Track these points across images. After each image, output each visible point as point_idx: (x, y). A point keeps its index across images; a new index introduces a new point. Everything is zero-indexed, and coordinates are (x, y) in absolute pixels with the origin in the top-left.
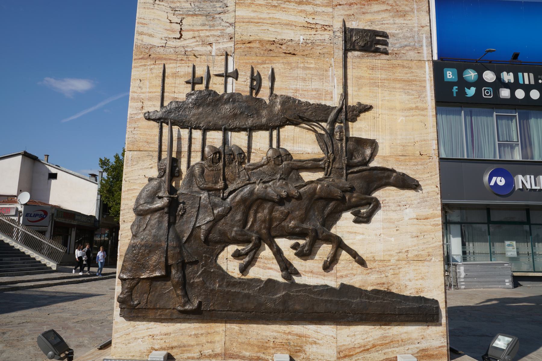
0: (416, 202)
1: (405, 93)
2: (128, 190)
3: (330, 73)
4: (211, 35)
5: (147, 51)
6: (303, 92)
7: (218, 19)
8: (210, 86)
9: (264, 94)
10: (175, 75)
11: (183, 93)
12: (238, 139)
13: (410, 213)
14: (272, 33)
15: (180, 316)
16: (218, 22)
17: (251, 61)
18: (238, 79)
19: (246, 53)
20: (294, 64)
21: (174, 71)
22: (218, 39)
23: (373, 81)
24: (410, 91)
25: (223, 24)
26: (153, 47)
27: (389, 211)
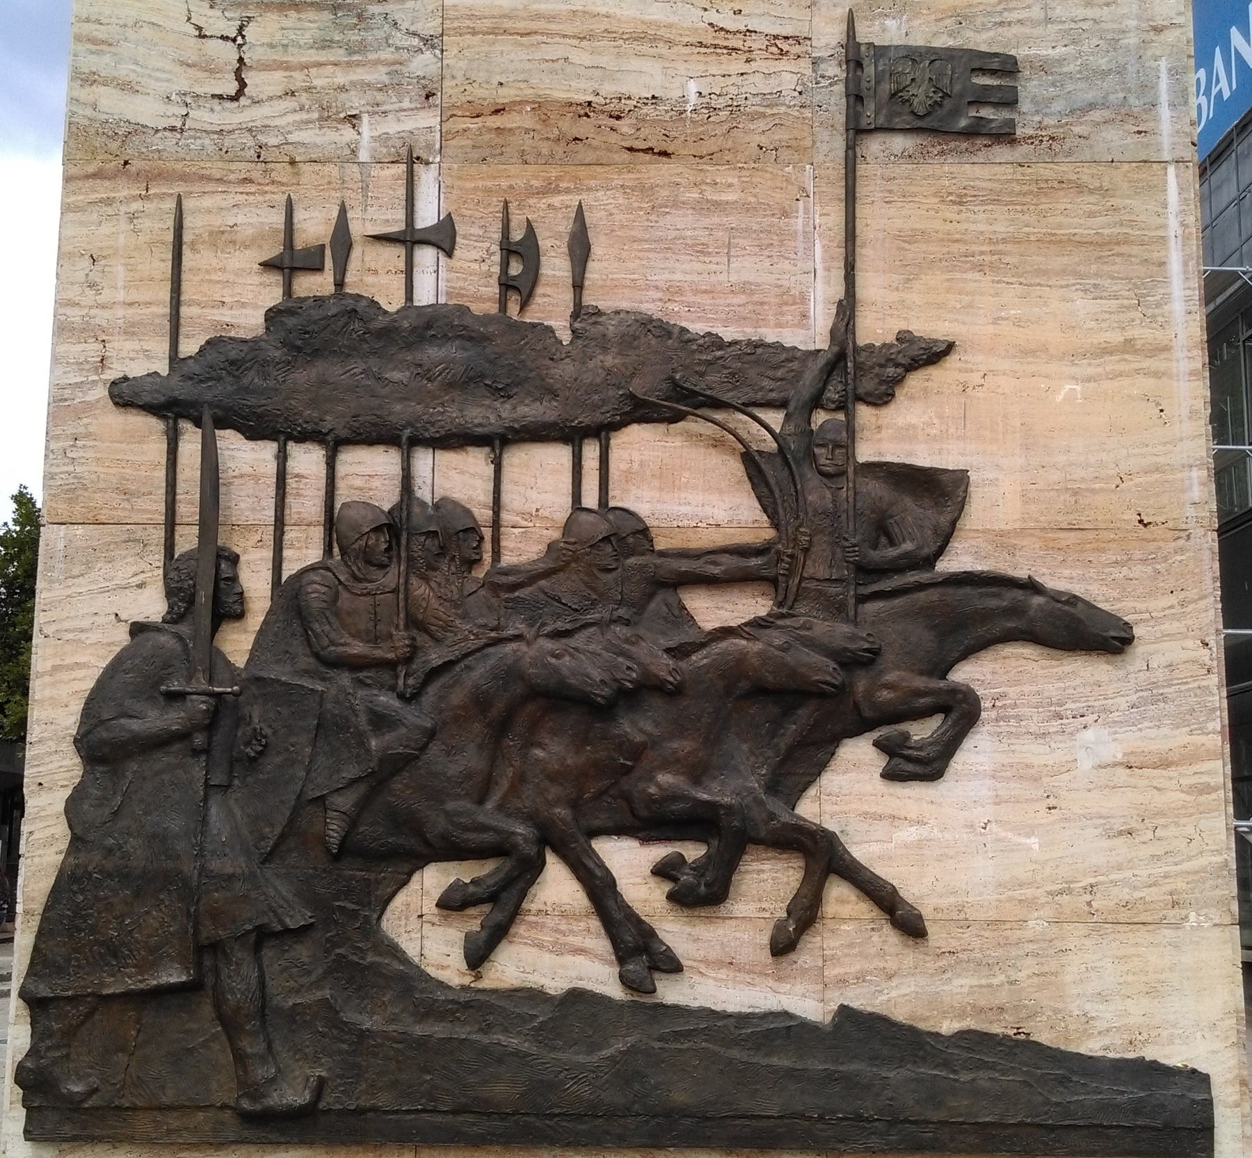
0: (1122, 702)
1: (1085, 291)
2: (56, 668)
3: (799, 223)
4: (353, 84)
5: (113, 146)
6: (698, 299)
7: (379, 20)
8: (349, 278)
9: (551, 308)
10: (223, 239)
11: (256, 307)
12: (454, 477)
13: (1099, 743)
14: (582, 71)
15: (246, 1133)
16: (380, 34)
17: (504, 184)
18: (457, 253)
19: (486, 152)
20: (665, 193)
21: (217, 222)
22: (380, 97)
23: (963, 248)
24: (1106, 283)
25: (399, 39)
26: (138, 129)
27: (1018, 736)
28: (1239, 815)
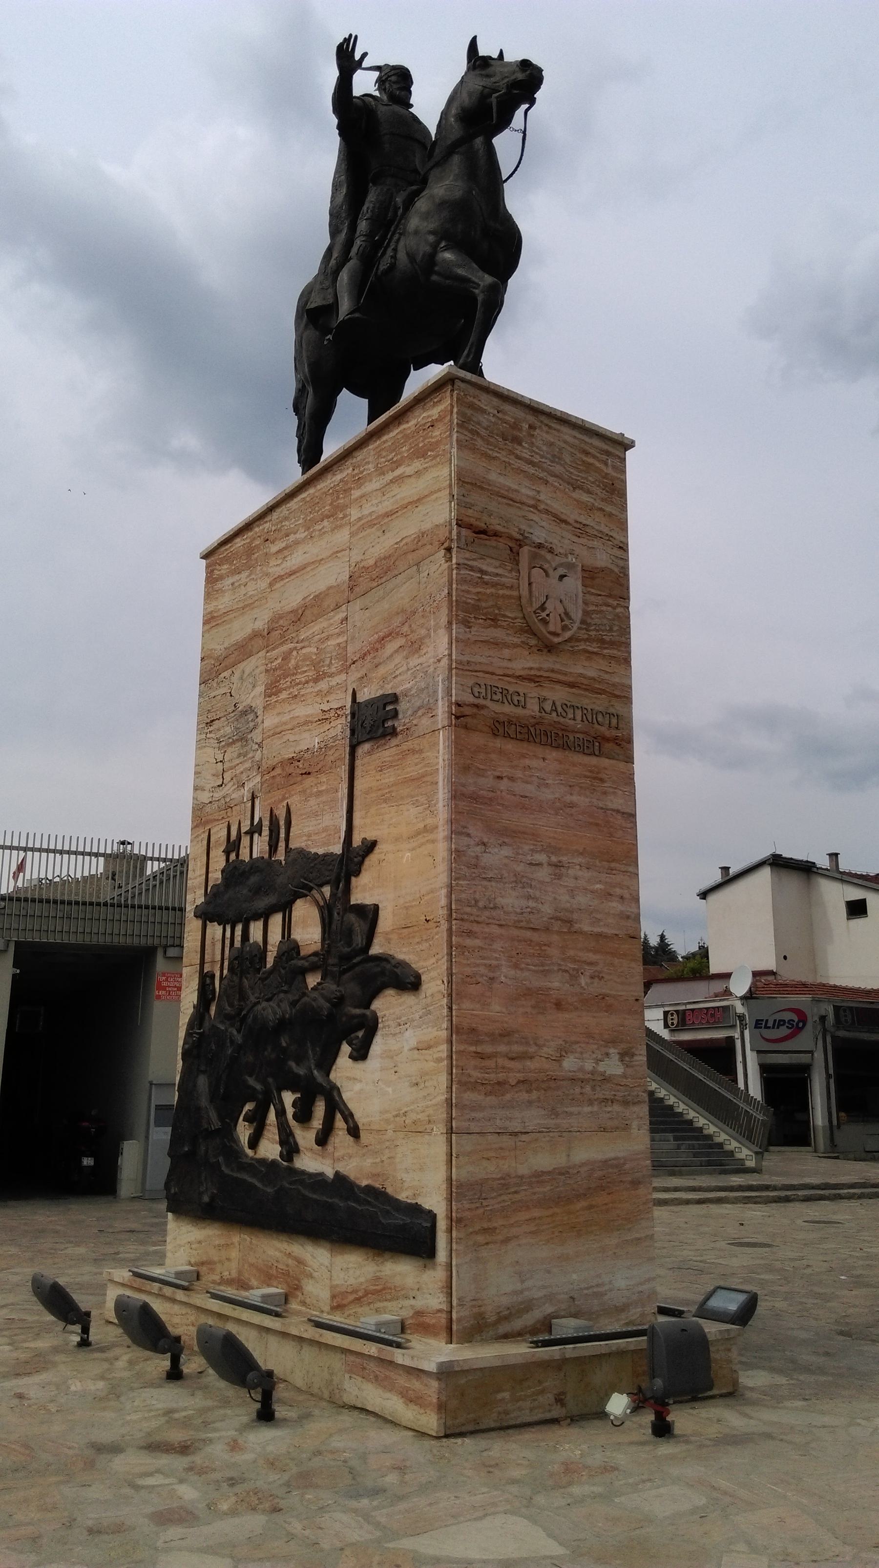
0: (417, 1016)
28: (101, 1184)
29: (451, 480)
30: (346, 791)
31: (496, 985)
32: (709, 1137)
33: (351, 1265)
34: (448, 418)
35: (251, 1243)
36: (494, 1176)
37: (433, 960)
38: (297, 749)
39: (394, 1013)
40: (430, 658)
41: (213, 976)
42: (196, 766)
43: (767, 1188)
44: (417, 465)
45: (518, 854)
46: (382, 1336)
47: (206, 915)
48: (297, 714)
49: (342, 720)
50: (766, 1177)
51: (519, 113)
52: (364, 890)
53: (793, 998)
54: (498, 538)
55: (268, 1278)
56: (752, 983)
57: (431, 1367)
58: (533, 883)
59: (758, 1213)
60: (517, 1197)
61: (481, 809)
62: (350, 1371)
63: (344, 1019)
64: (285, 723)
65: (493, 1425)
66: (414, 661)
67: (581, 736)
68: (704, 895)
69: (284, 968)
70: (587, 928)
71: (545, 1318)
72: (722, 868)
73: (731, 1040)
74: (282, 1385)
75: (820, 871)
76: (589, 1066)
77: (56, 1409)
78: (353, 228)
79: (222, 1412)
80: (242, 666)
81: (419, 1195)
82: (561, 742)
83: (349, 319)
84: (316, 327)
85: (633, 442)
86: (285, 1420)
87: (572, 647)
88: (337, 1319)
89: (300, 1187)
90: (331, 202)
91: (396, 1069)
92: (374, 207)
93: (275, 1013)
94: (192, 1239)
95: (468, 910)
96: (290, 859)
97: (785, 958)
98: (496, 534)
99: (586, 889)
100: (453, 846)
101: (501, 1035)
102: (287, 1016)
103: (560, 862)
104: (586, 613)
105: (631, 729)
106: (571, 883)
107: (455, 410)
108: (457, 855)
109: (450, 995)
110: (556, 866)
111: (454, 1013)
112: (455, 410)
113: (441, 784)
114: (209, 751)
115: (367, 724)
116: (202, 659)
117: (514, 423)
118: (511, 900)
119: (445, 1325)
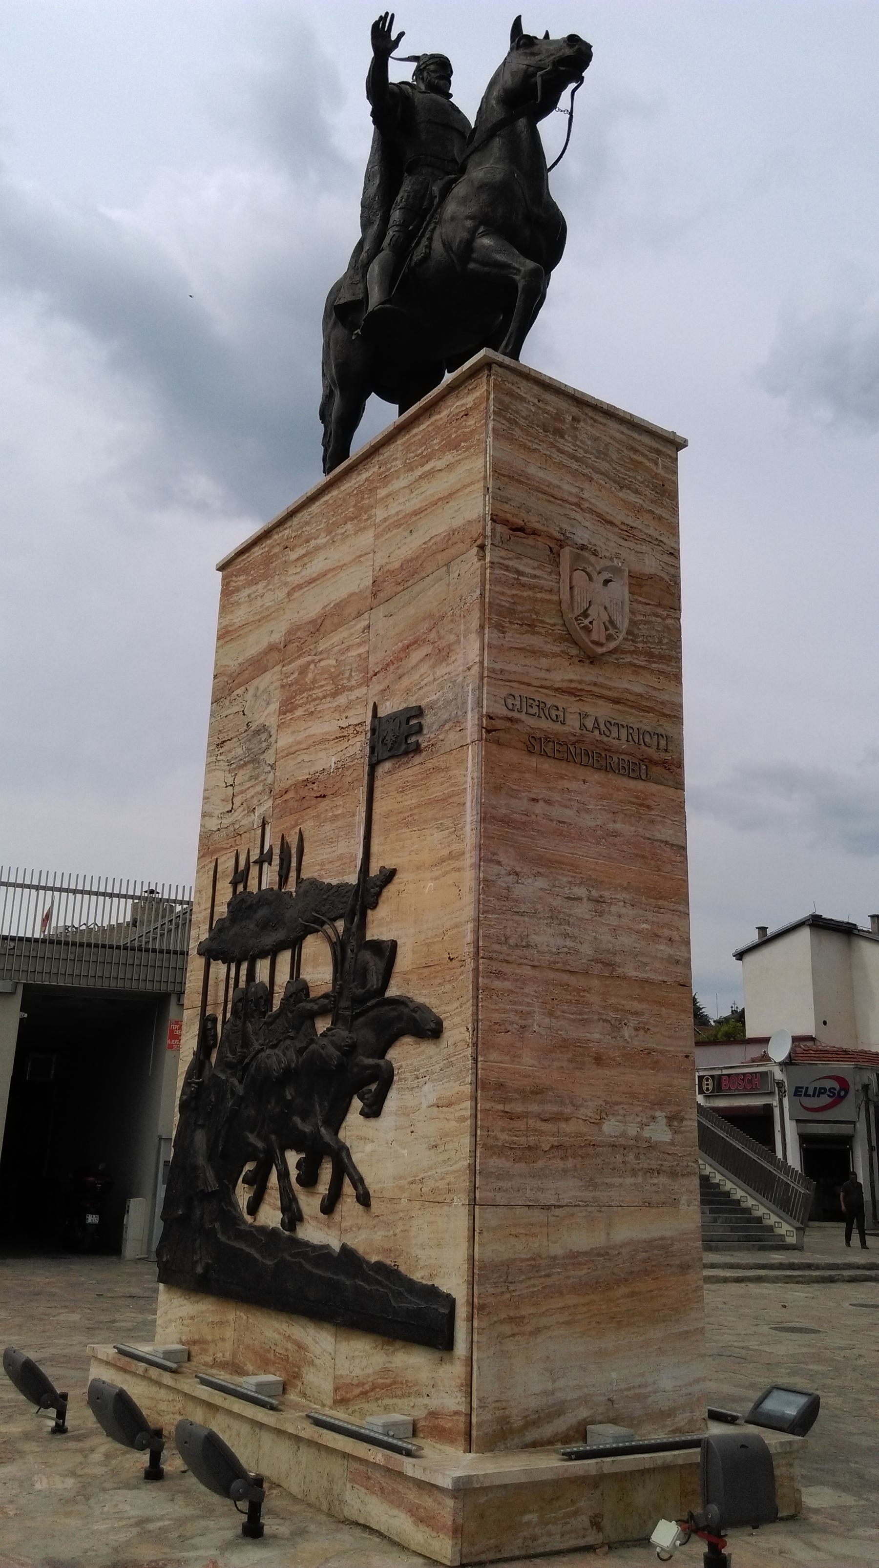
0: (437, 1068)
1: (437, 828)
28: (106, 1244)
29: (486, 471)
30: (364, 815)
31: (527, 1035)
32: (748, 1211)
33: (357, 1353)
34: (484, 405)
35: (247, 1322)
36: (523, 1256)
37: (457, 1004)
38: (312, 771)
39: (411, 1064)
40: (459, 666)
41: (215, 1020)
42: (205, 790)
43: (809, 1267)
44: (449, 457)
45: (554, 886)
46: (390, 1440)
47: (209, 953)
48: (312, 733)
49: (362, 738)
50: (809, 1254)
51: (566, 95)
52: (381, 925)
53: (835, 1065)
54: (536, 537)
55: (265, 1364)
56: (792, 1048)
57: (446, 1482)
58: (571, 920)
59: (801, 1294)
60: (549, 1281)
61: (513, 833)
62: (353, 1481)
63: (355, 1070)
64: (299, 743)
65: (517, 1553)
66: (441, 671)
67: (626, 758)
68: (740, 956)
69: (292, 1012)
70: (632, 973)
71: (579, 1423)
72: (759, 928)
73: (769, 1108)
74: (275, 1492)
75: (861, 934)
76: (632, 1130)
77: (14, 1512)
78: (386, 219)
79: (203, 1523)
80: (256, 682)
81: (436, 1275)
82: (604, 764)
83: (379, 309)
84: (344, 325)
85: (686, 441)
86: (275, 1536)
87: (617, 659)
88: (340, 1416)
89: (303, 1262)
90: (364, 193)
91: (412, 1128)
92: (408, 197)
93: (280, 1062)
94: (184, 1314)
95: (497, 947)
96: (301, 890)
97: (825, 1023)
98: (535, 532)
99: (630, 929)
100: (481, 875)
101: (532, 1092)
102: (293, 1065)
103: (601, 897)
104: (632, 623)
105: (681, 753)
106: (615, 922)
107: (492, 396)
108: (485, 885)
109: (475, 1045)
110: (598, 901)
111: (479, 1066)
112: (492, 396)
113: (468, 804)
114: (220, 774)
115: (389, 742)
116: (215, 677)
117: (557, 414)
118: (545, 938)
119: (463, 1430)
